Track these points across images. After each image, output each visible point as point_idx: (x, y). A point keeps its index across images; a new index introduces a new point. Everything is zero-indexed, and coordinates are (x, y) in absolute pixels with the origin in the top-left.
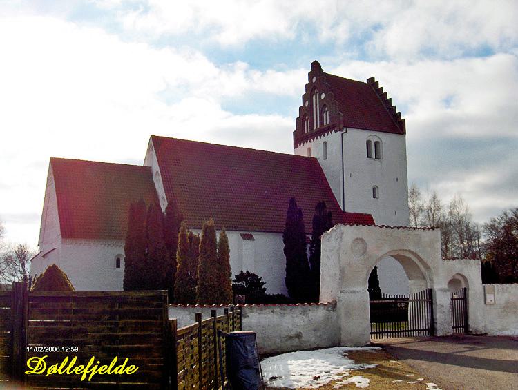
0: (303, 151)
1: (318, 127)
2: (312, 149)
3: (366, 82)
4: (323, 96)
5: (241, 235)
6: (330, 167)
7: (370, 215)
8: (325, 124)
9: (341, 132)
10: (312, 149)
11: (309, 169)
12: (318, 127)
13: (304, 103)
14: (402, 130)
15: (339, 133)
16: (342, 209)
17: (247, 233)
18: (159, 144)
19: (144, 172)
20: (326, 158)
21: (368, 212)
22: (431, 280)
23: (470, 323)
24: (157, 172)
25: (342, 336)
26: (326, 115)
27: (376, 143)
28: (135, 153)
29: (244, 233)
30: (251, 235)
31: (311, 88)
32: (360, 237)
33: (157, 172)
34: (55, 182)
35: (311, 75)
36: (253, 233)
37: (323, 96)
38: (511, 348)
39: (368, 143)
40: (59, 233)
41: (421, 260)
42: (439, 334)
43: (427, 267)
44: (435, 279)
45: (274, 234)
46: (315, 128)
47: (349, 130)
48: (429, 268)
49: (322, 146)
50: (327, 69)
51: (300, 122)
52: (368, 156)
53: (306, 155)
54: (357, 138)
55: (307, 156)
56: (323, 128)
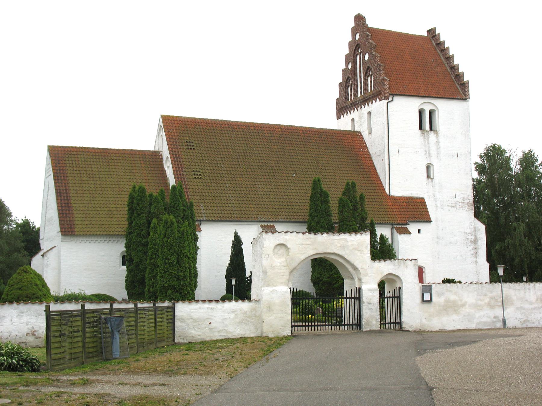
0: (344, 124)
1: (363, 94)
2: (355, 121)
3: (426, 34)
4: (367, 57)
5: (262, 226)
6: (374, 144)
7: (423, 199)
8: (369, 91)
9: (386, 101)
10: (355, 121)
11: (350, 146)
12: (363, 94)
13: (347, 65)
14: (465, 94)
15: (385, 102)
16: (388, 192)
17: (269, 224)
18: (173, 126)
19: (154, 157)
20: (370, 133)
21: (421, 196)
22: (360, 280)
23: (405, 319)
24: (168, 157)
25: (264, 328)
26: (371, 79)
27: (431, 113)
28: (147, 138)
29: (266, 224)
30: (273, 227)
31: (355, 49)
32: (278, 243)
33: (168, 157)
34: (54, 173)
35: (354, 31)
36: (275, 224)
37: (367, 57)
38: (115, 309)
39: (421, 113)
40: (58, 229)
41: (348, 262)
42: (365, 328)
43: (355, 269)
44: (364, 279)
45: (300, 224)
46: (359, 95)
47: (396, 99)
48: (357, 268)
49: (366, 115)
50: (371, 23)
51: (344, 87)
52: (421, 128)
53: (349, 128)
54: (404, 110)
55: (350, 129)
56: (367, 95)
